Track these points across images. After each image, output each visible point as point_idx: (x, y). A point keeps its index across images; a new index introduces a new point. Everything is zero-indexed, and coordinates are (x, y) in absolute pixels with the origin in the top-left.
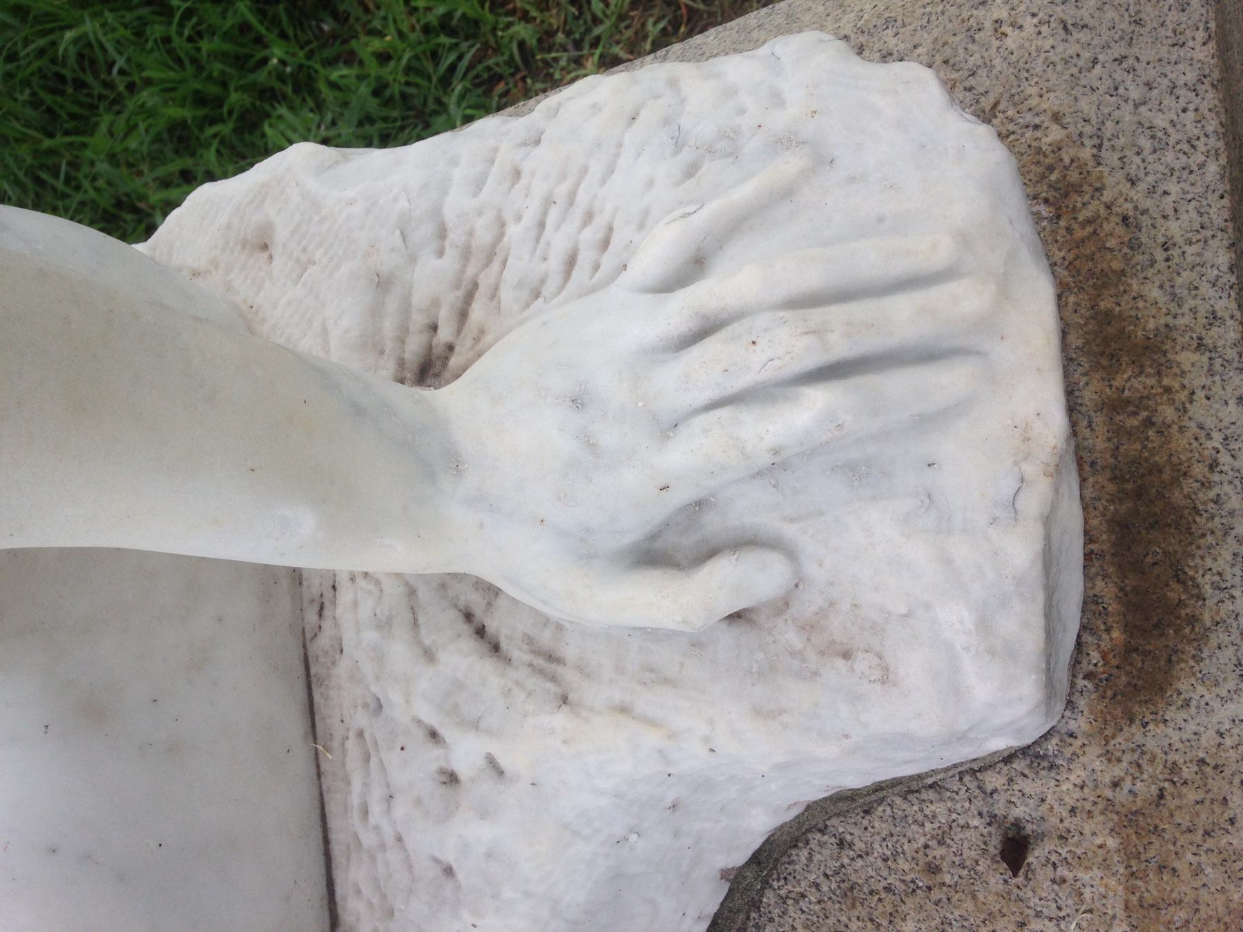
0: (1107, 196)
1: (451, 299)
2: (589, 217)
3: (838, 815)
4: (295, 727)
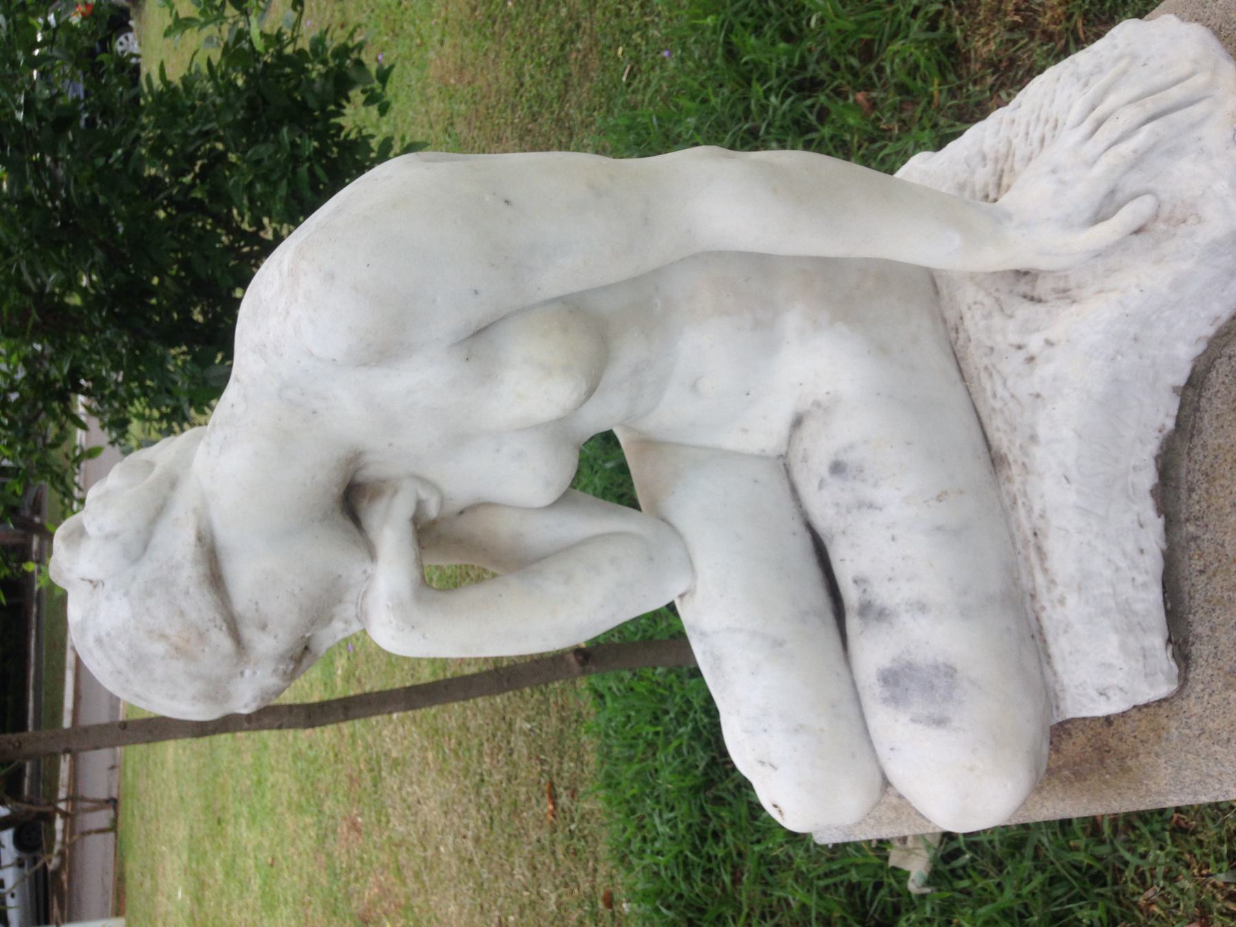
3: (1225, 346)
4: (955, 375)
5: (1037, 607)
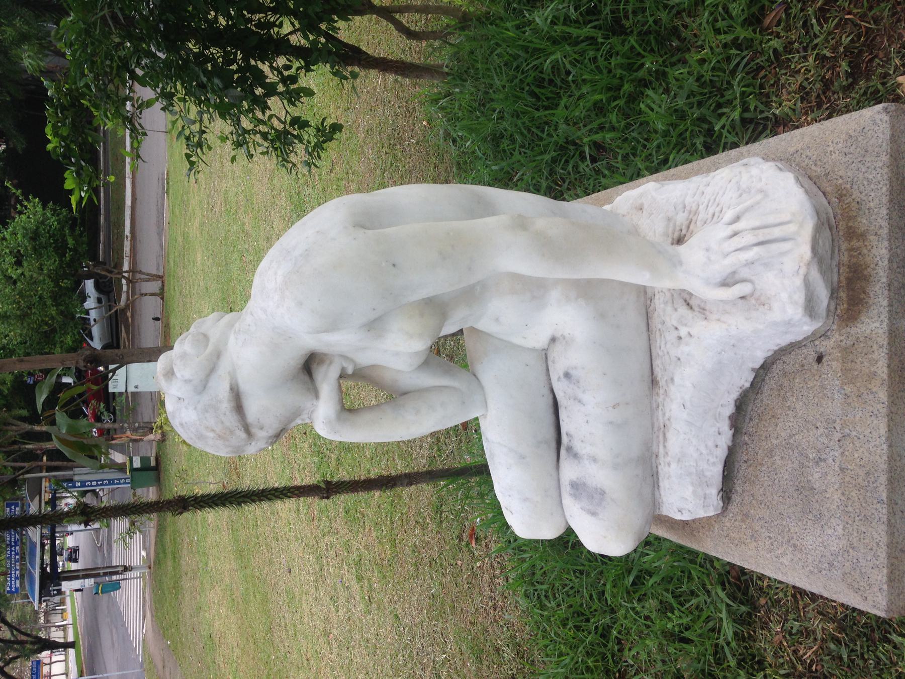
0: (853, 197)
1: (686, 223)
2: (718, 205)
4: (644, 328)
5: (658, 462)
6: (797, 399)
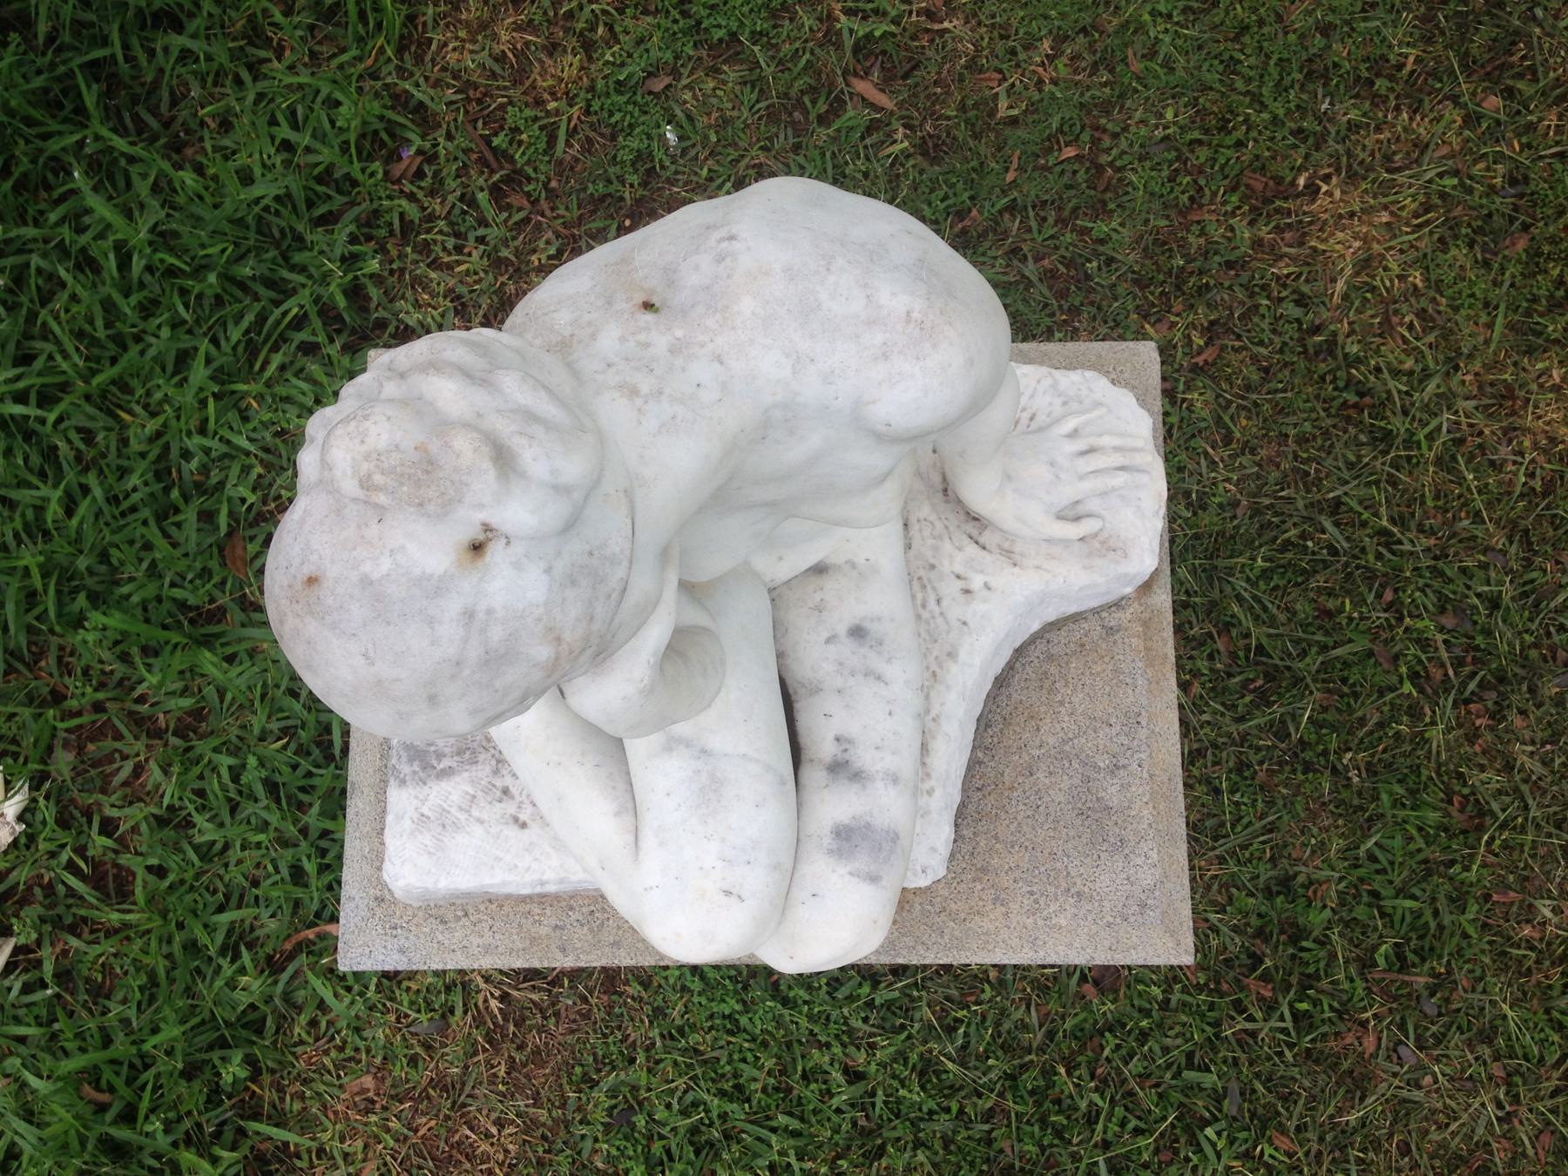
6: (1074, 690)
